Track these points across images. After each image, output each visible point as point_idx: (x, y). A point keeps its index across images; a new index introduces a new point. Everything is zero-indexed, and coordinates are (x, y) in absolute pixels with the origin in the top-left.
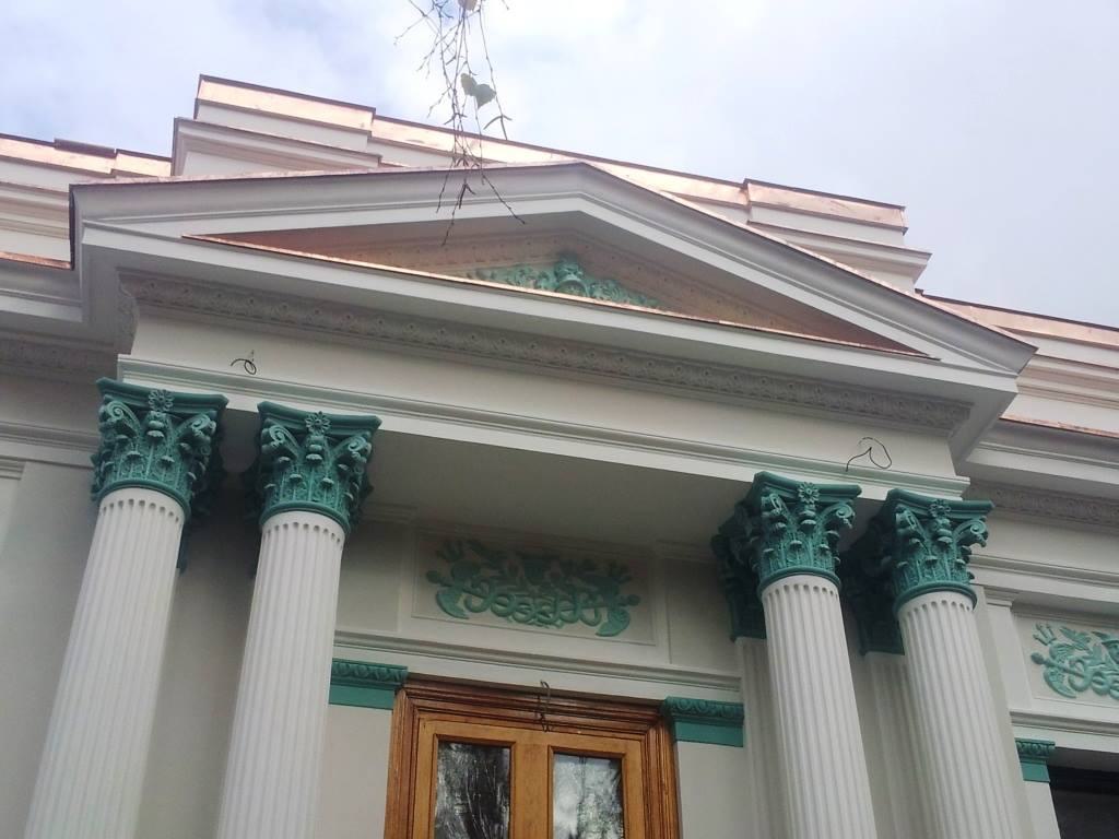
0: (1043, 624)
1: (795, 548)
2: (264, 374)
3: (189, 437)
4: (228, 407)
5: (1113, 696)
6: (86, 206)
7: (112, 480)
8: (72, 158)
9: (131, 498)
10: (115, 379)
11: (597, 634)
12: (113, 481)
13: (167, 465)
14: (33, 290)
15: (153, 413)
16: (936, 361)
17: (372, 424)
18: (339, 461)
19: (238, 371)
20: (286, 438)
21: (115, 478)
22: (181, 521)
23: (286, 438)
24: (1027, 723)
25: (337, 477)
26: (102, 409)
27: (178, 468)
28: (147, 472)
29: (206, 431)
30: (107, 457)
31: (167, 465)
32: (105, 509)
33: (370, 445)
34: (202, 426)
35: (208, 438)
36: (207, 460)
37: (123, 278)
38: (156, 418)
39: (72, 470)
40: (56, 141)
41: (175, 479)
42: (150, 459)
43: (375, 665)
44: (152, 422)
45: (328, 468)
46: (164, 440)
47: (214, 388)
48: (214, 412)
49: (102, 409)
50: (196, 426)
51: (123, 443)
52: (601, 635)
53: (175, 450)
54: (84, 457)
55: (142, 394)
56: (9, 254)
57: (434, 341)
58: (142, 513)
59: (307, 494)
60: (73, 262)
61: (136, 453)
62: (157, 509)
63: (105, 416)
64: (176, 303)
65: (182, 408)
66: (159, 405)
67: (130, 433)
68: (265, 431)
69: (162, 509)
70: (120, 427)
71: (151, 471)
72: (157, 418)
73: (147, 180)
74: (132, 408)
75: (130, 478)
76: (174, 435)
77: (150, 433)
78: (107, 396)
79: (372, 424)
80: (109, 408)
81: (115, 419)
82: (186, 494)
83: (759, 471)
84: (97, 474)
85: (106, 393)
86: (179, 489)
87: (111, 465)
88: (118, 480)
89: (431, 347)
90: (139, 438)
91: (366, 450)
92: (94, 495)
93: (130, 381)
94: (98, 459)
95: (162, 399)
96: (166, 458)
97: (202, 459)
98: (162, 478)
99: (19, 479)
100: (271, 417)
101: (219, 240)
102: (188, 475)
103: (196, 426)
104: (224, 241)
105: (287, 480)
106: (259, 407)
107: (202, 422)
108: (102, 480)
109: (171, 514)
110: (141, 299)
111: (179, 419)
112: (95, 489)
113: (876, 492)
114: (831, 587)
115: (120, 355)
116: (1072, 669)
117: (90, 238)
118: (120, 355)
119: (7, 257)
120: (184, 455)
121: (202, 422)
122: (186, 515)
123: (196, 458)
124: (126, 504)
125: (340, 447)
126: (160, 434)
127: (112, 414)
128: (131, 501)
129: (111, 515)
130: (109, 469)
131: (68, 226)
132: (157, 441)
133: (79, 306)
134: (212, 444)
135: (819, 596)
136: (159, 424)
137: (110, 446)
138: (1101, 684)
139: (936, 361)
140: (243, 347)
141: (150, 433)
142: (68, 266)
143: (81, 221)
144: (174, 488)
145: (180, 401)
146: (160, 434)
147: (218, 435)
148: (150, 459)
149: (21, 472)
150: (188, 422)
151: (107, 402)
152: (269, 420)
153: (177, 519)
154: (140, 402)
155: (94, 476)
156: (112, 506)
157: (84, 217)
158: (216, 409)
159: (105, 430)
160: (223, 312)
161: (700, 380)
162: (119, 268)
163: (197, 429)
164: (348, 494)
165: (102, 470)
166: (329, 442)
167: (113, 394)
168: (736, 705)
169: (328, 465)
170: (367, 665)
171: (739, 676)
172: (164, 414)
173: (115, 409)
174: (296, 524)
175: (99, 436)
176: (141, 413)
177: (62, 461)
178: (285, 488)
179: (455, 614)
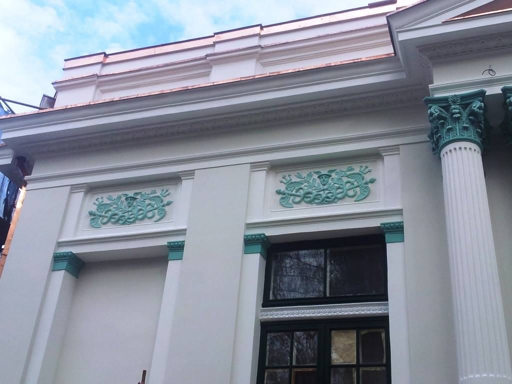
0: (286, 174)
1: (449, 130)
2: (500, 74)
3: (473, 113)
4: (486, 94)
5: (315, 203)
6: (395, 24)
7: (442, 142)
8: (378, 9)
9: (460, 146)
10: (429, 96)
11: (355, 201)
12: (442, 144)
13: (466, 128)
14: (385, 70)
15: (453, 106)
16: (445, 23)
17: (482, 94)
18: (470, 115)
19: (487, 76)
20: (440, 111)
21: (444, 140)
22: (480, 153)
23: (440, 111)
24: (372, 217)
25: (470, 123)
26: (429, 111)
27: (471, 128)
28: (458, 134)
29: (480, 108)
30: (437, 133)
31: (466, 128)
32: (444, 155)
33: (483, 104)
34: (477, 106)
35: (482, 111)
36: (483, 122)
37: (420, 51)
38: (454, 109)
39: (421, 144)
40: (369, 4)
41: (471, 134)
42: (457, 128)
43: (398, 223)
44: (454, 111)
45: (464, 120)
46: (461, 118)
47: (469, 89)
48: (481, 98)
49: (429, 111)
50: (474, 107)
51: (443, 124)
52: (358, 201)
53: (468, 121)
54: (425, 137)
55: (445, 99)
56: (367, 58)
57: (497, 45)
58: (456, 154)
59: (457, 134)
60: (395, 53)
61: (450, 127)
62: (468, 149)
63: (431, 114)
64: (447, 55)
65: (465, 101)
66: (454, 102)
67: (445, 119)
68: (508, 100)
69: (470, 149)
70: (440, 117)
71: (460, 133)
72: (455, 109)
73: (404, 8)
74: (443, 107)
75: (451, 138)
76: (465, 115)
77: (454, 116)
78: (429, 105)
79: (482, 94)
80: (432, 110)
81: (436, 114)
82: (478, 140)
83: (503, 86)
84: (433, 143)
85: (429, 103)
86: (475, 138)
87: (440, 136)
88: (445, 141)
89: (439, 57)
90: (449, 120)
91: (481, 107)
92: (434, 152)
93: (438, 95)
94: (431, 136)
95: (455, 99)
96: (465, 125)
97: (481, 123)
98: (466, 135)
99: (399, 154)
100: (510, 93)
101: (460, 18)
102: (477, 131)
103: (474, 107)
104: (462, 18)
105: (446, 130)
106: (502, 90)
107: (476, 105)
108: (436, 145)
109: (475, 150)
110: (431, 58)
111: (465, 106)
112: (434, 150)
113: (496, 90)
114: (474, 146)
115: (429, 86)
116: (298, 193)
117: (402, 37)
118: (429, 86)
119: (367, 59)
120: (472, 122)
121: (476, 105)
122: (481, 150)
123: (478, 122)
124: (453, 151)
125: (468, 109)
126: (459, 115)
127: (434, 112)
128: (455, 149)
129: (447, 157)
130: (438, 140)
131: (390, 39)
132: (458, 118)
133: (403, 71)
134: (484, 114)
135: (456, 154)
136: (457, 111)
137: (437, 127)
138: (310, 197)
139: (445, 23)
140: (485, 65)
141: (454, 116)
142: (393, 55)
143: (394, 31)
144: (472, 138)
145: (463, 97)
146: (459, 115)
147: (485, 109)
148: (457, 128)
149: (399, 151)
150: (470, 106)
151: (430, 108)
152: (509, 95)
153: (478, 152)
154: (445, 103)
155: (431, 144)
156: (447, 153)
157: (396, 29)
158: (481, 97)
159: (431, 121)
160: (438, 56)
161: (497, 44)
162: (417, 47)
163: (475, 108)
164: (478, 130)
165: (435, 139)
166: (462, 107)
167: (431, 103)
168: (400, 223)
169: (464, 118)
170: (393, 223)
171: (399, 207)
172: (458, 106)
173: (435, 109)
174: (460, 148)
175: (429, 125)
176: (447, 108)
177: (423, 140)
178: (445, 134)
179: (288, 206)
